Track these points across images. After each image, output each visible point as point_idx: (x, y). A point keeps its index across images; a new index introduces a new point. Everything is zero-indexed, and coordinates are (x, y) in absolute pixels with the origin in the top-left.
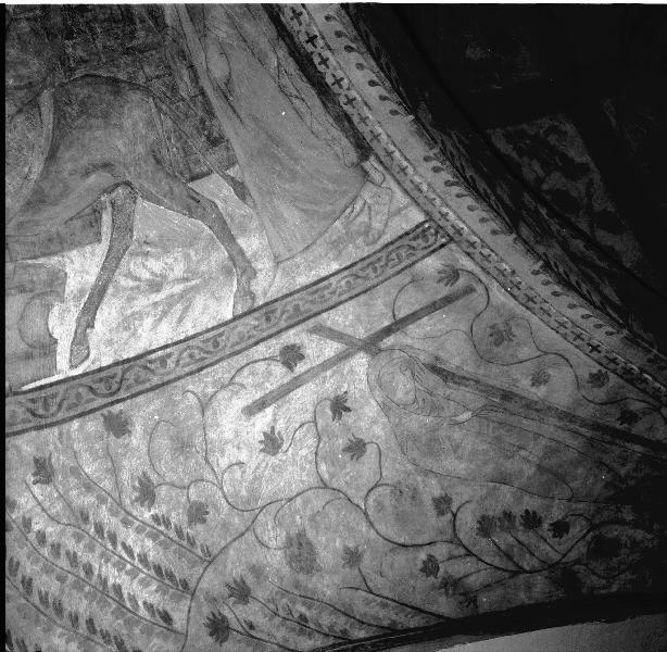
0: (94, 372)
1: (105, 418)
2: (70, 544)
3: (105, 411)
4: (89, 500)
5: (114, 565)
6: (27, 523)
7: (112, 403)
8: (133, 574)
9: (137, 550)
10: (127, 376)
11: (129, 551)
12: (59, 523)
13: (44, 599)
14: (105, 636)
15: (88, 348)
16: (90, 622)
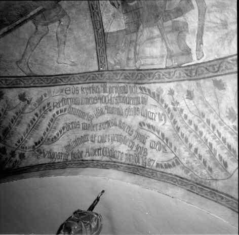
0: (207, 62)
1: (214, 81)
2: (195, 121)
3: (213, 78)
4: (206, 110)
5: (212, 136)
6: (182, 111)
7: (216, 76)
8: (218, 143)
9: (223, 135)
10: (221, 65)
11: (220, 135)
12: (193, 114)
13: (182, 135)
14: (200, 157)
15: (203, 53)
16: (196, 150)
